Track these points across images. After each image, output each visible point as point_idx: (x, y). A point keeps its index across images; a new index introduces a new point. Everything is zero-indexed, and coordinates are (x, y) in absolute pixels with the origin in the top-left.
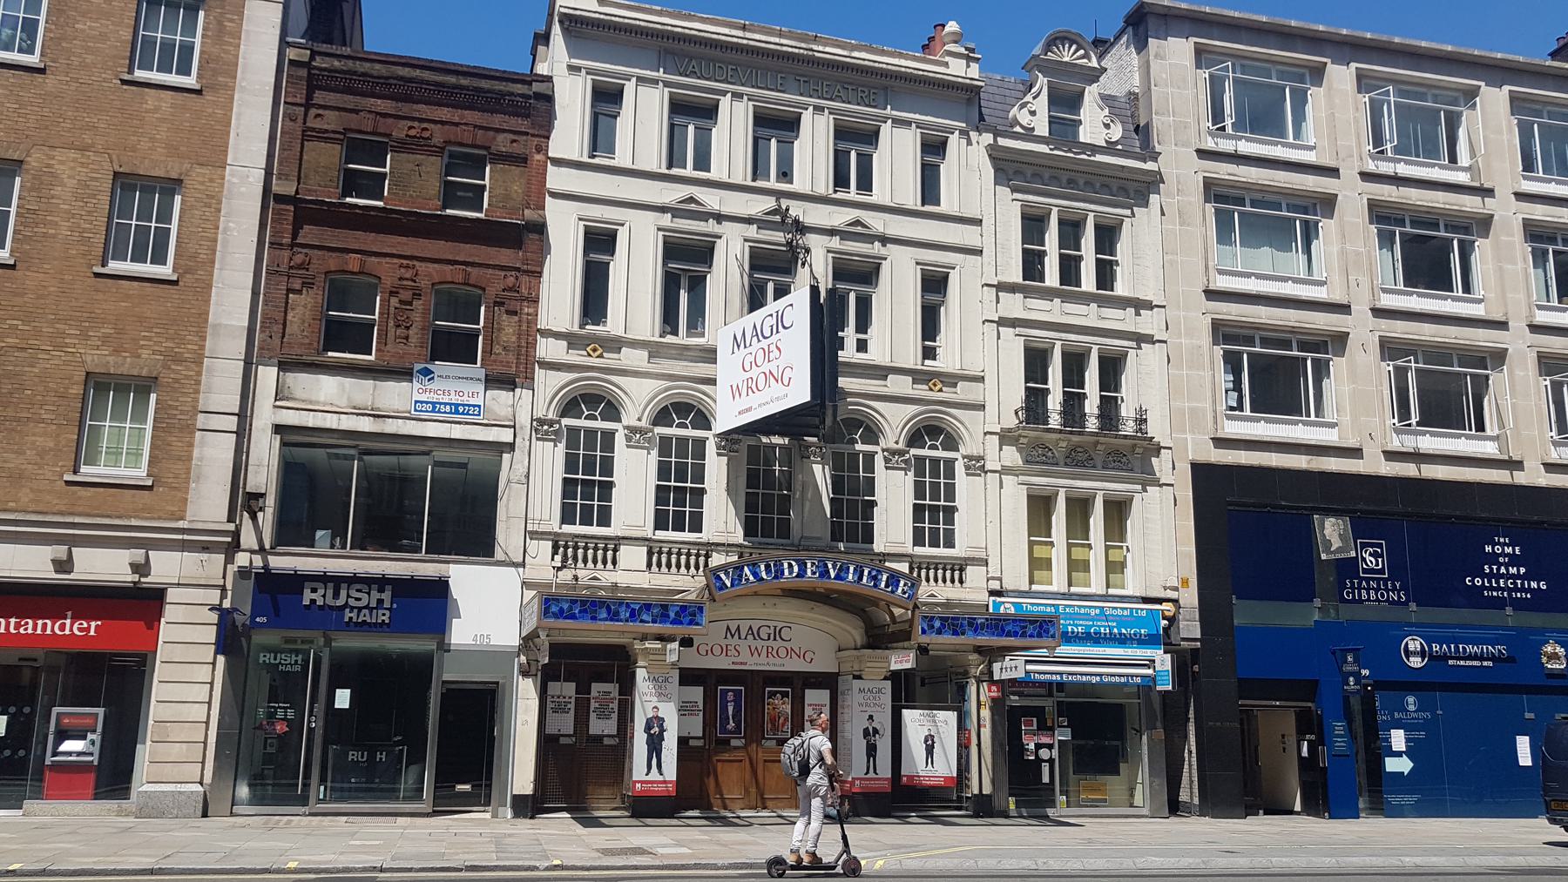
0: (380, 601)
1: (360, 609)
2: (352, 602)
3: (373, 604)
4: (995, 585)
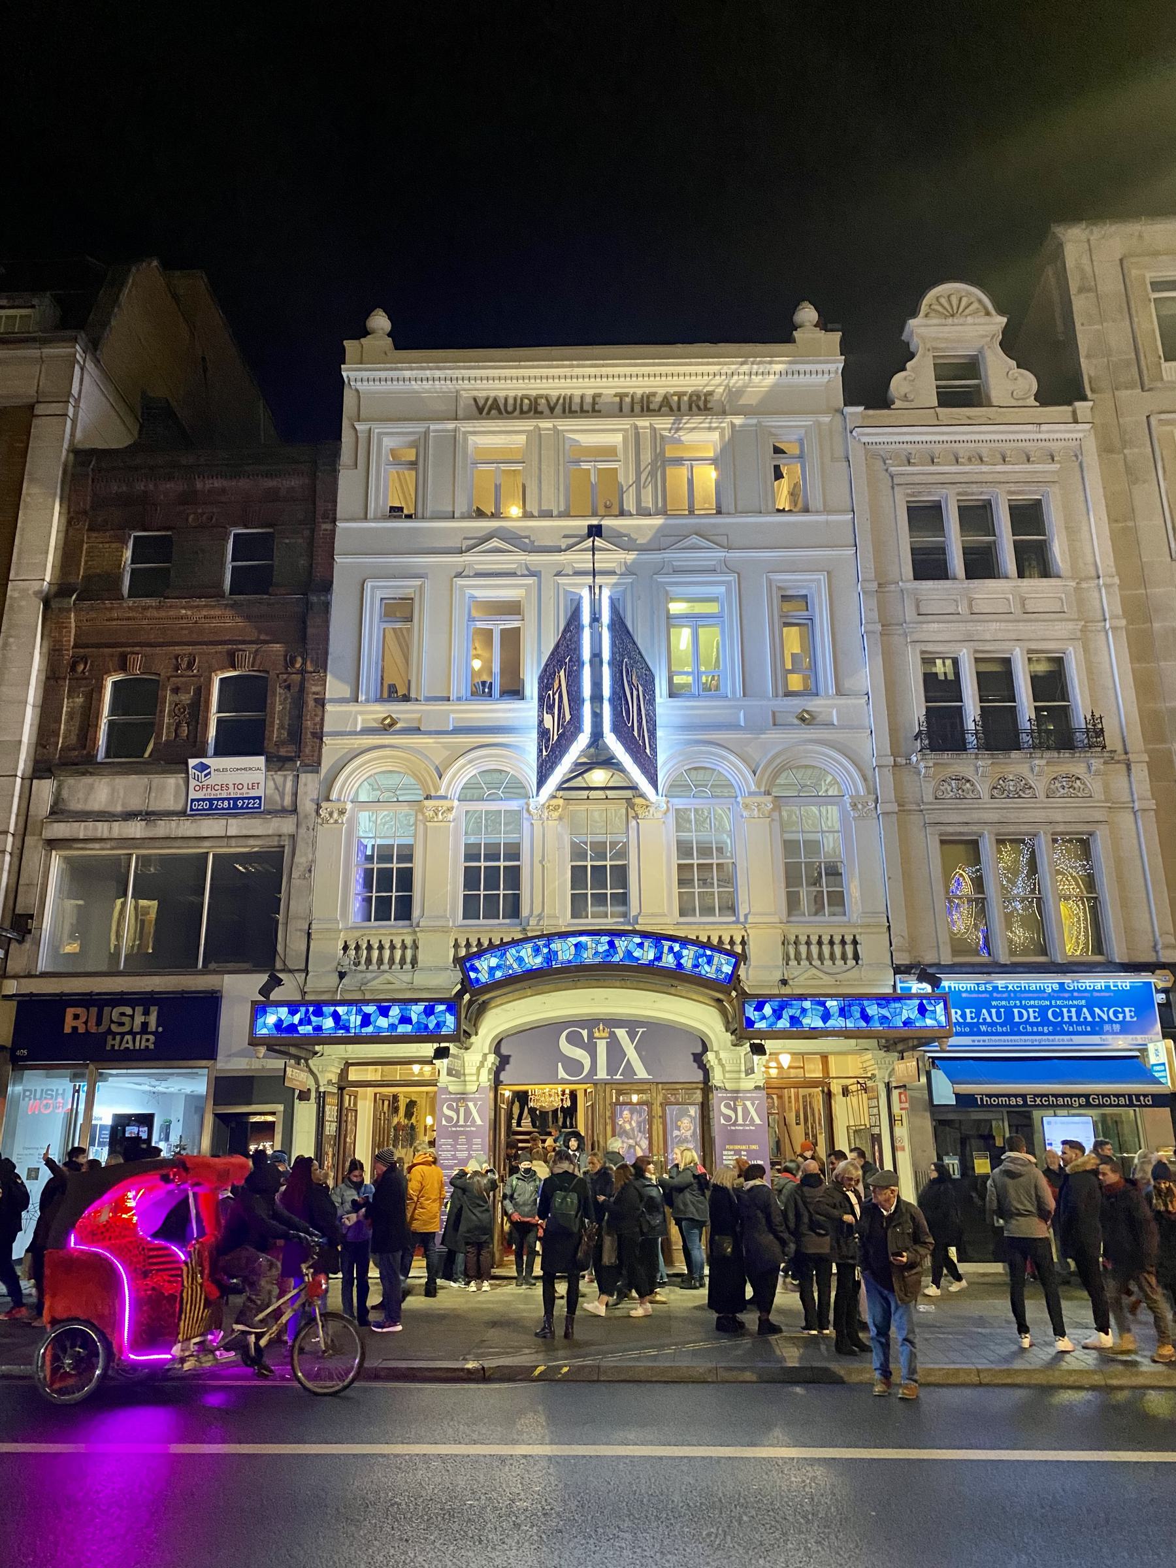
4: (902, 959)
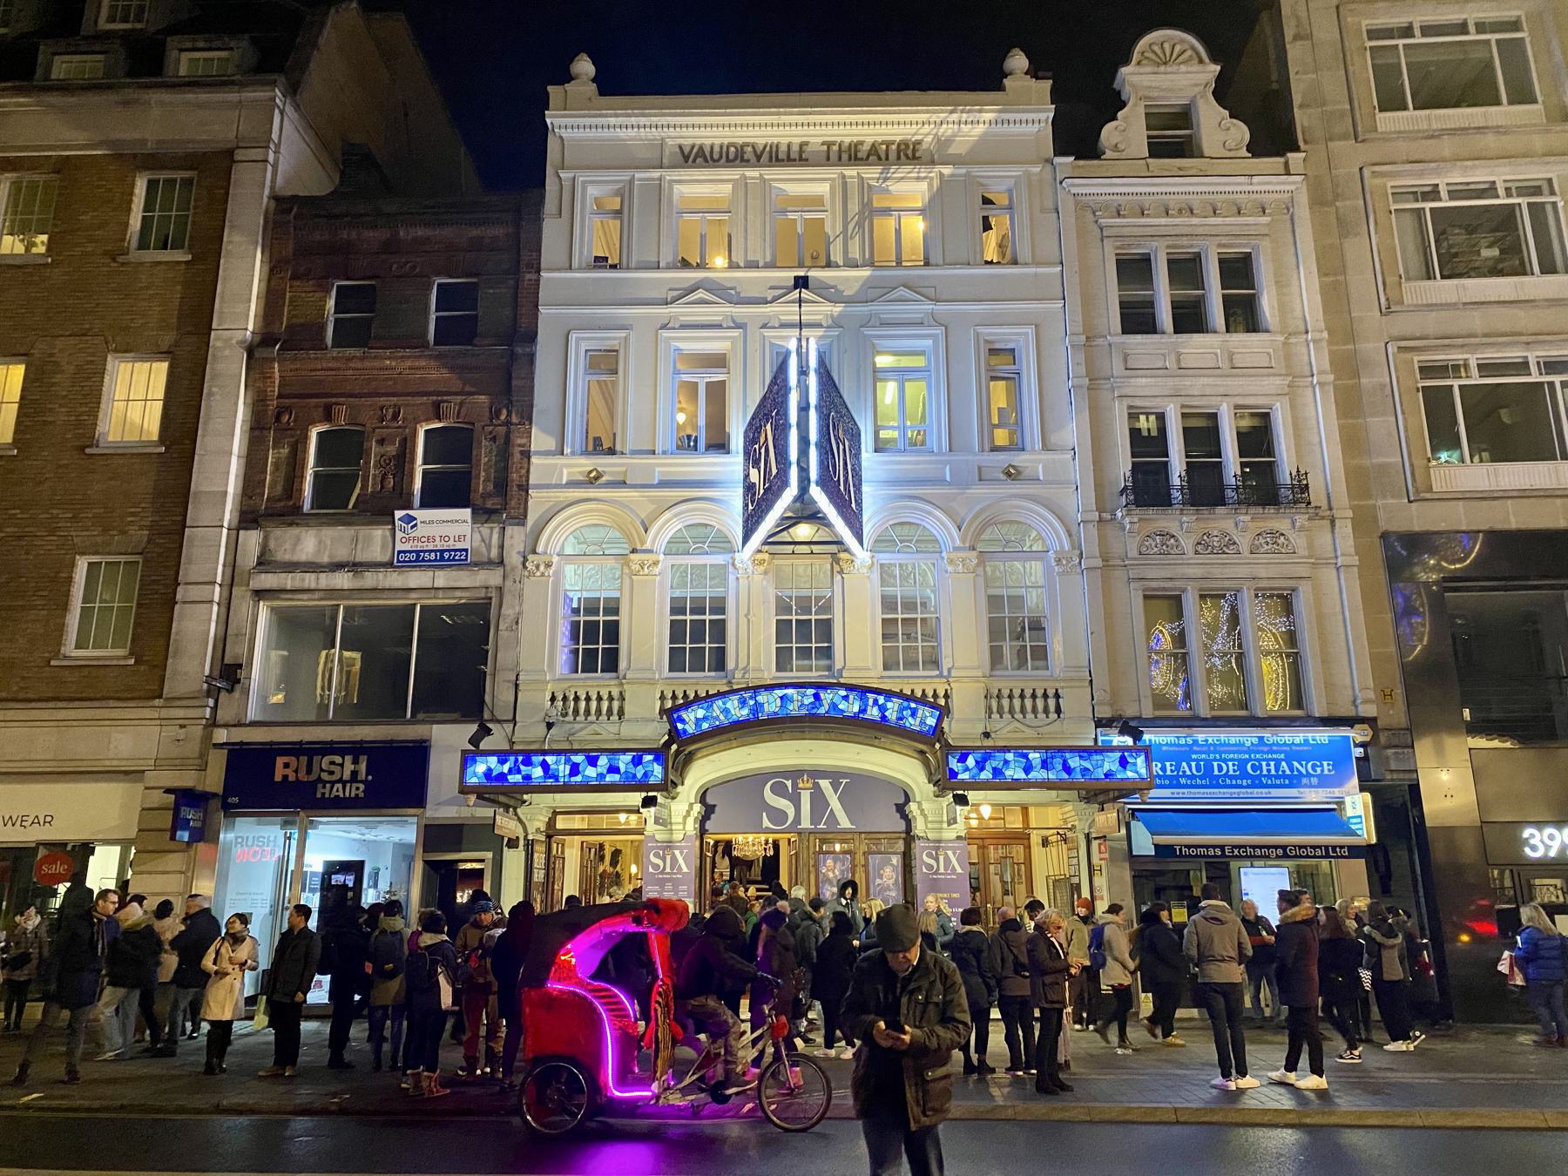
0: (354, 773)
1: (333, 783)
2: (325, 776)
3: (347, 776)
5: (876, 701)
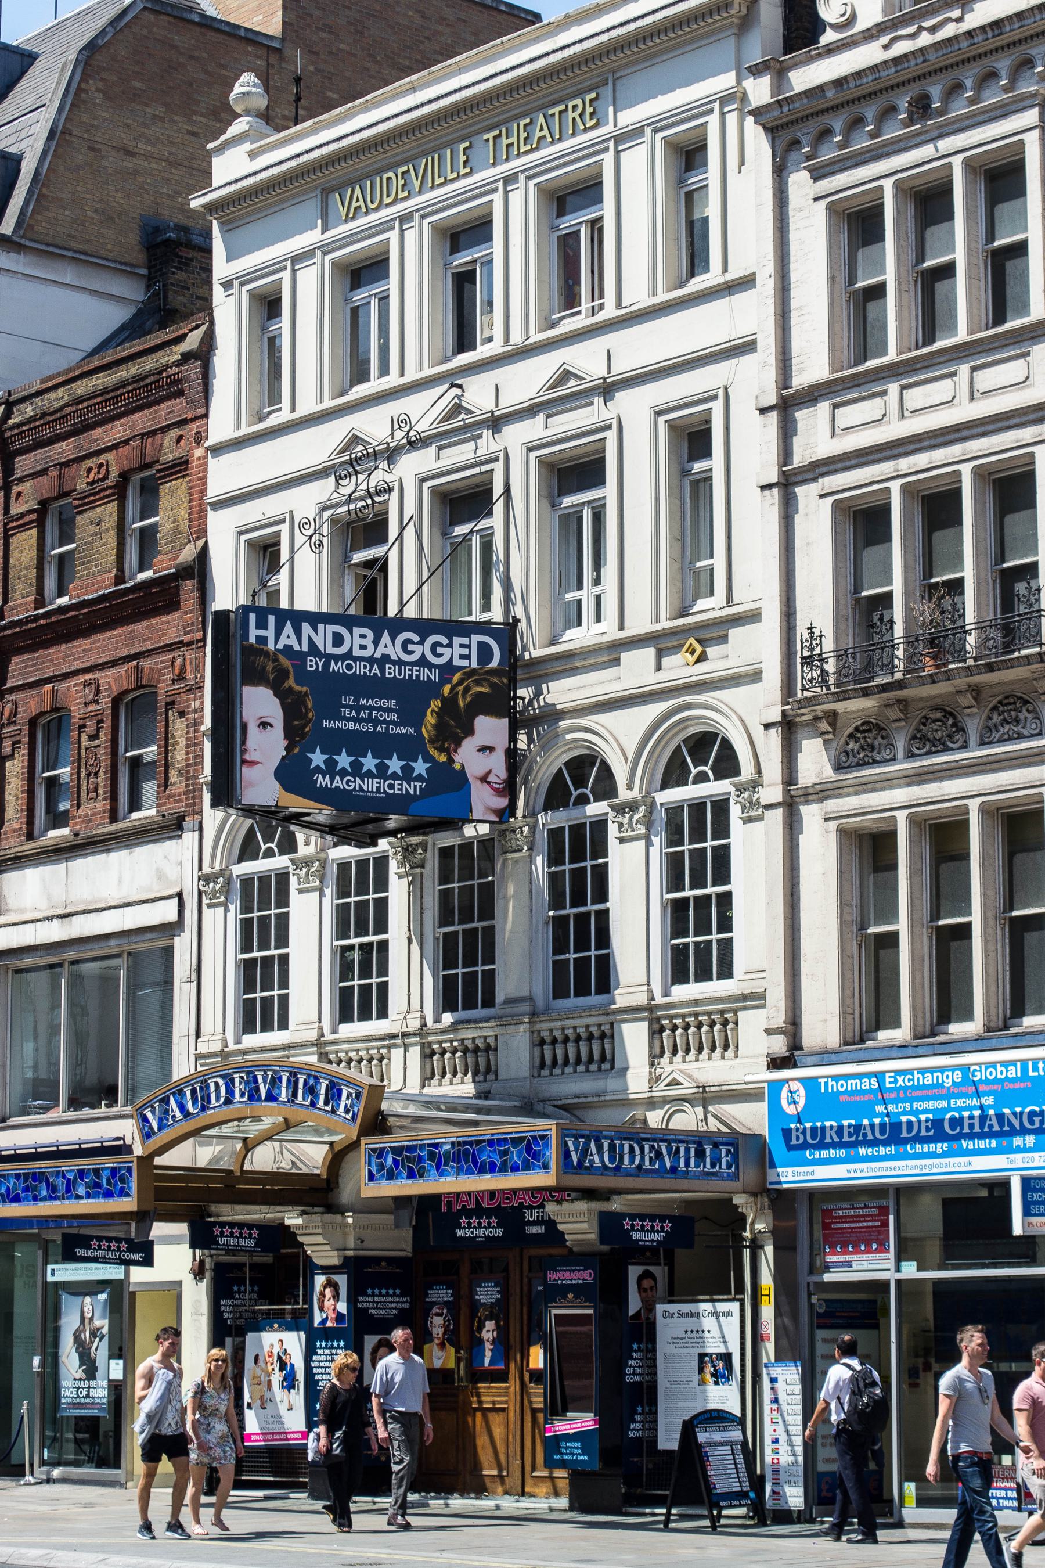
5: (306, 1083)
